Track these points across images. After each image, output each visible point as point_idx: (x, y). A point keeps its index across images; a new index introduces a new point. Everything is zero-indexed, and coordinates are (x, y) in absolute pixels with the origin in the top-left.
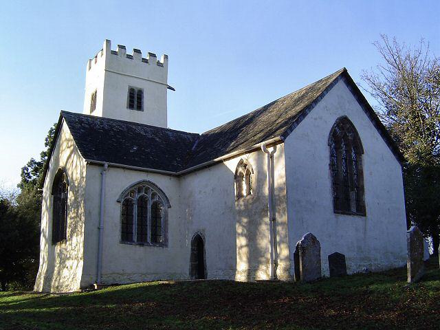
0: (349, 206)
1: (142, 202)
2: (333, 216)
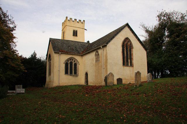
0: (128, 64)
1: (71, 63)
2: (122, 67)
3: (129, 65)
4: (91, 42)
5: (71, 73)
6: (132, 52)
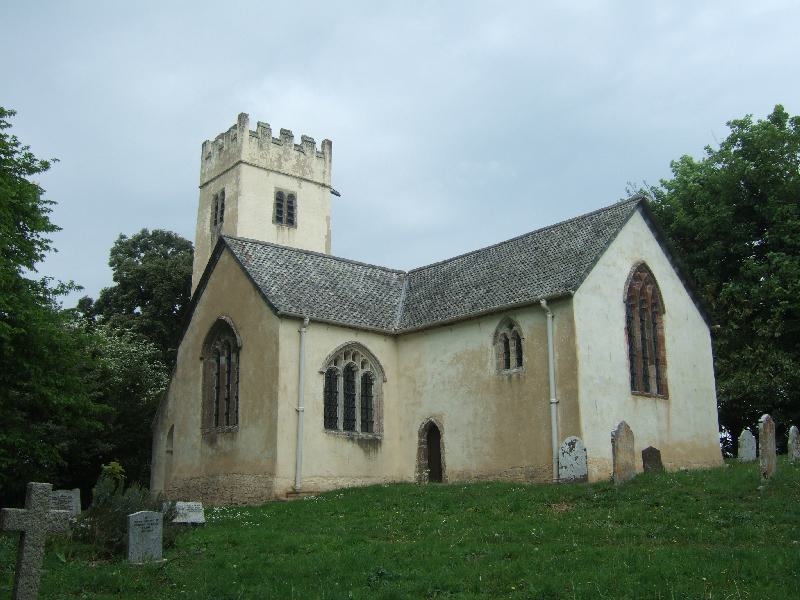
1: (350, 372)
3: (654, 389)
4: (130, 237)
5: (349, 425)
6: (660, 332)
